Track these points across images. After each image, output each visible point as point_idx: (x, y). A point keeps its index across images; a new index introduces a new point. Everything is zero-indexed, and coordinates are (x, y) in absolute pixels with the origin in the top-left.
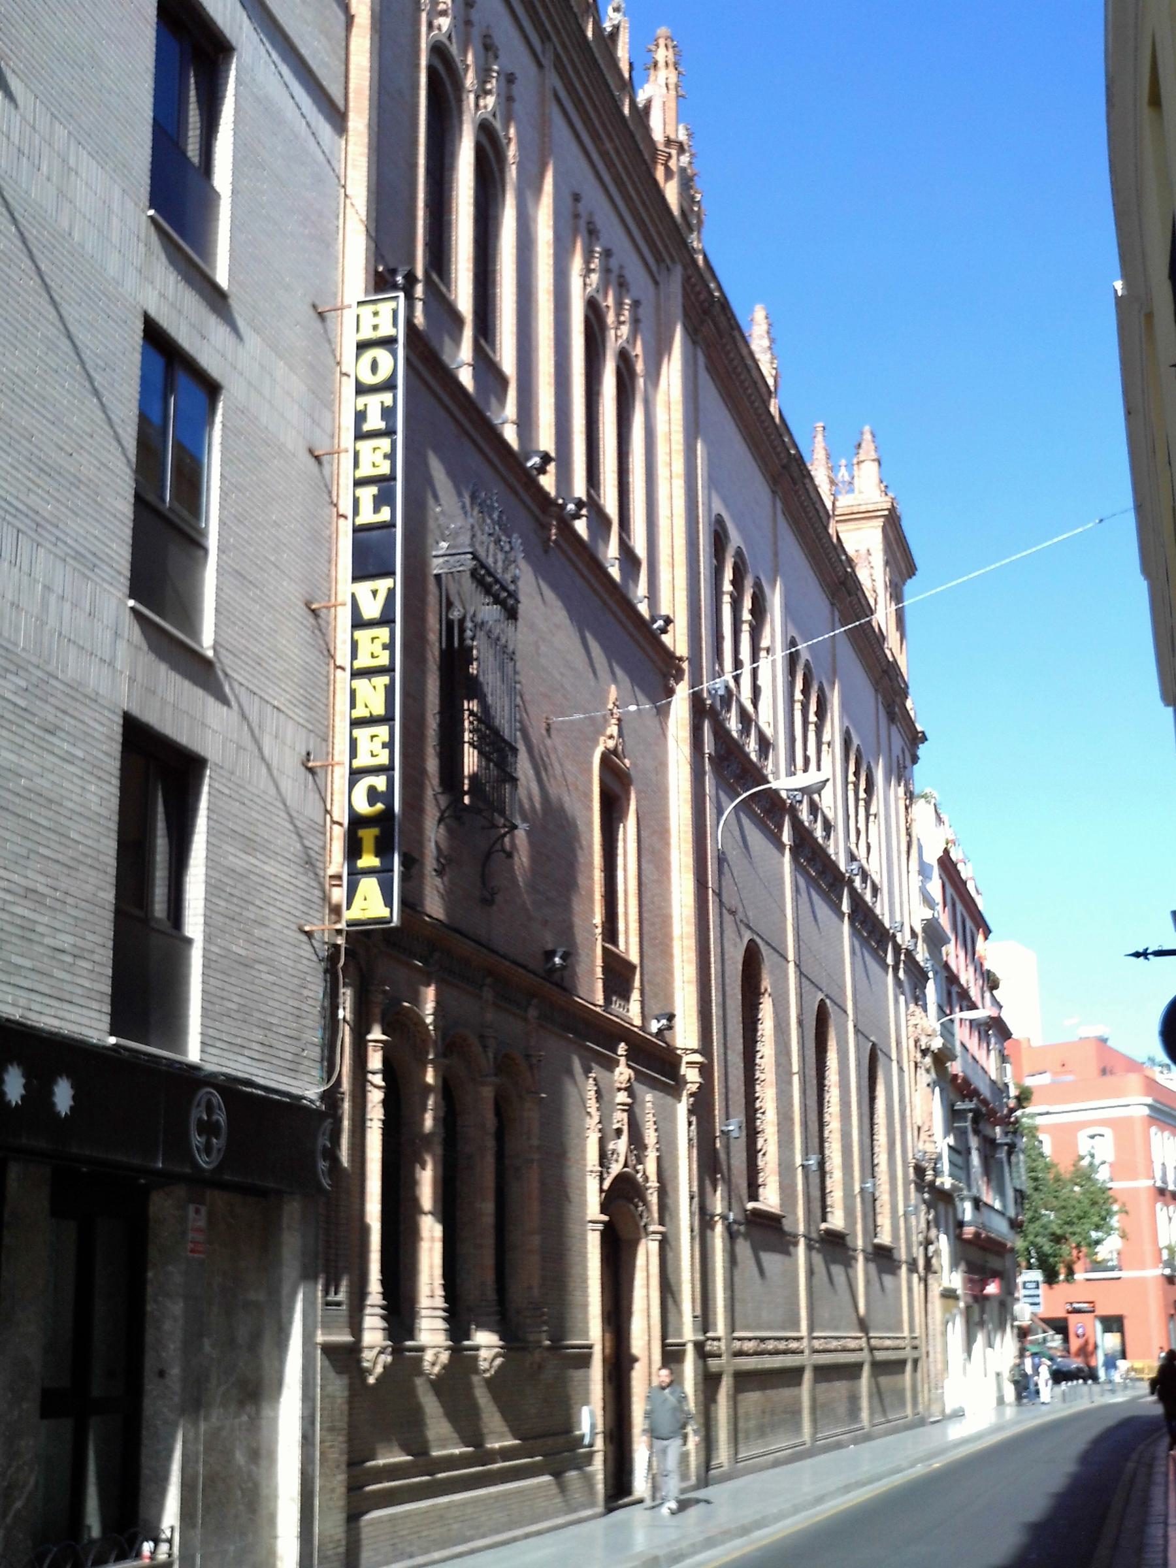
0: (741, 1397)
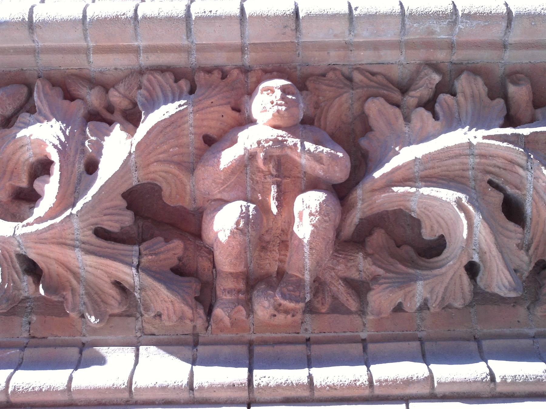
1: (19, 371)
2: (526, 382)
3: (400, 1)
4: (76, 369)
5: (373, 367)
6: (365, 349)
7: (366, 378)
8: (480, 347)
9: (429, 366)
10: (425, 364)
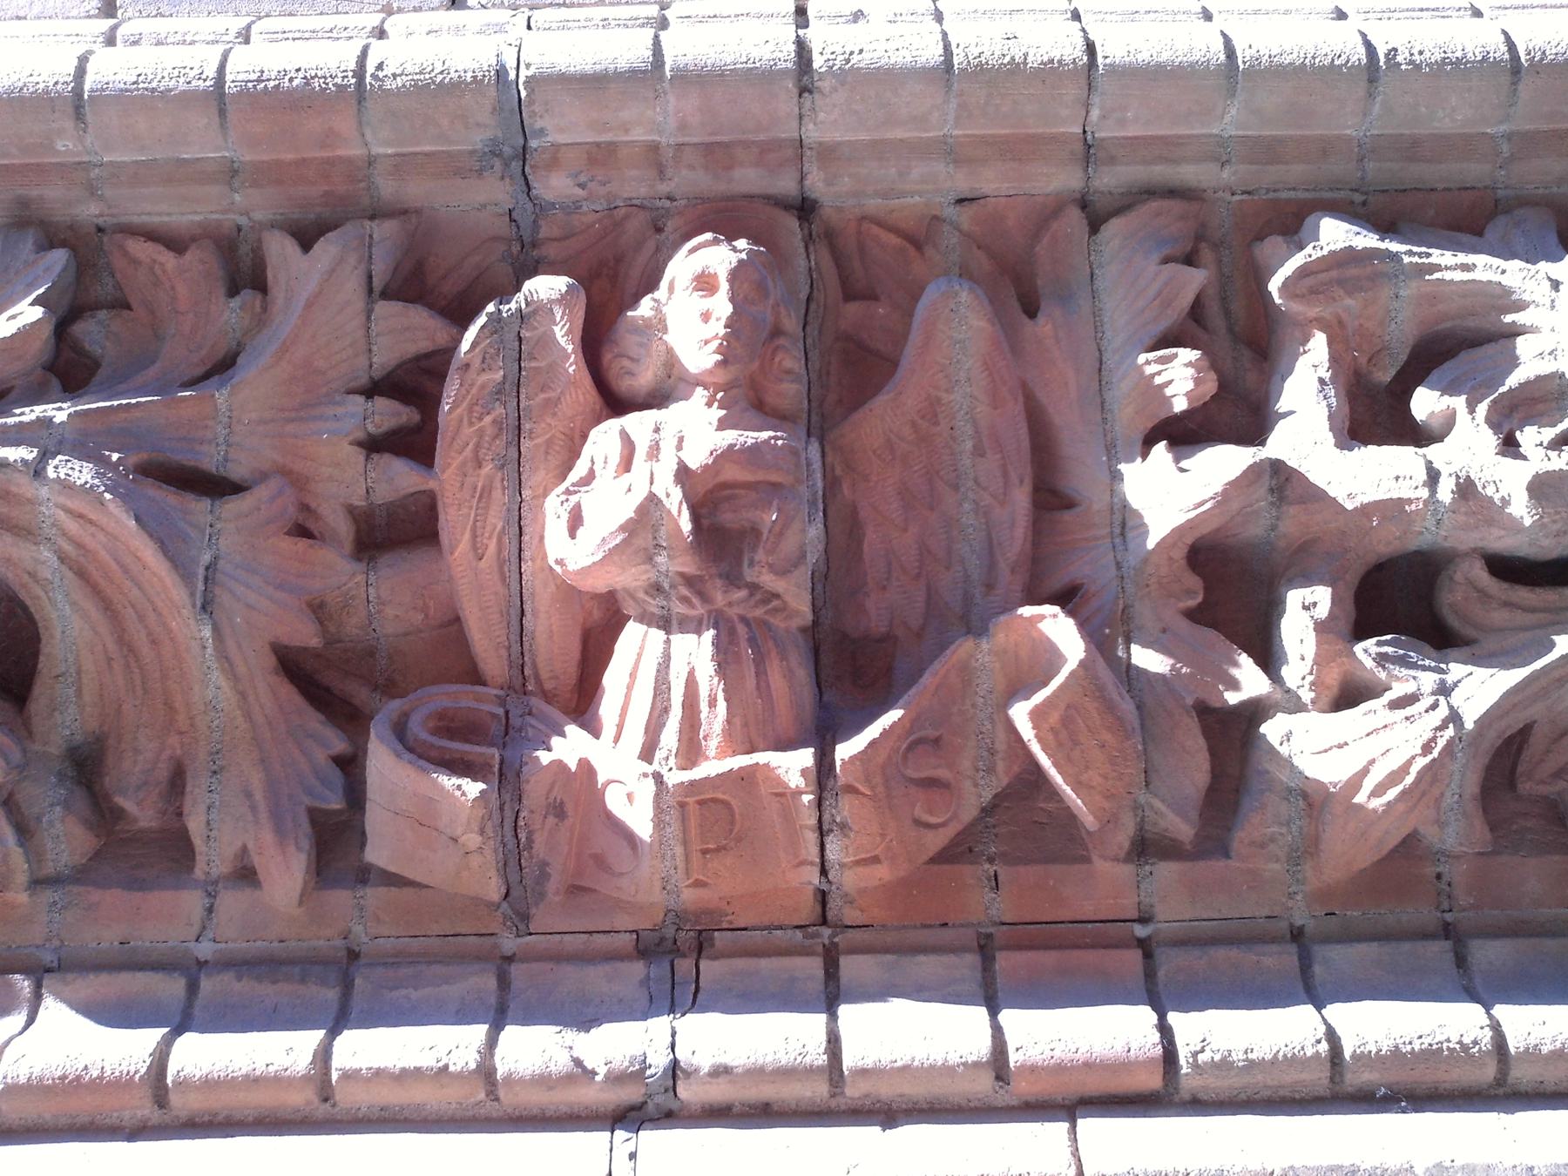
1: (346, 1033)
2: (1431, 1055)
3: (1359, 31)
4: (178, 1030)
5: (1007, 1017)
6: (193, 988)
7: (1486, 1036)
8: (1461, 961)
9: (1323, 1011)
10: (1310, 1007)
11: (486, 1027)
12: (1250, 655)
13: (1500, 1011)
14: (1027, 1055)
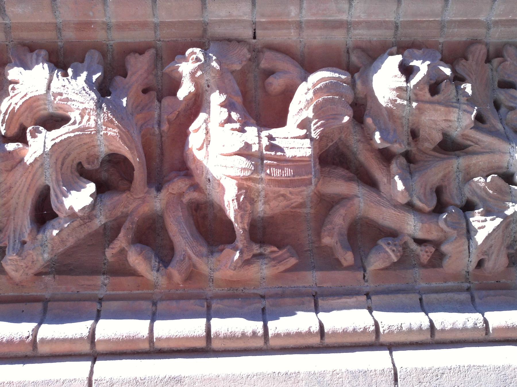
0: (318, 315)
10: (314, 313)
11: (149, 321)
12: (8, 143)
13: (431, 315)
14: (464, 326)
